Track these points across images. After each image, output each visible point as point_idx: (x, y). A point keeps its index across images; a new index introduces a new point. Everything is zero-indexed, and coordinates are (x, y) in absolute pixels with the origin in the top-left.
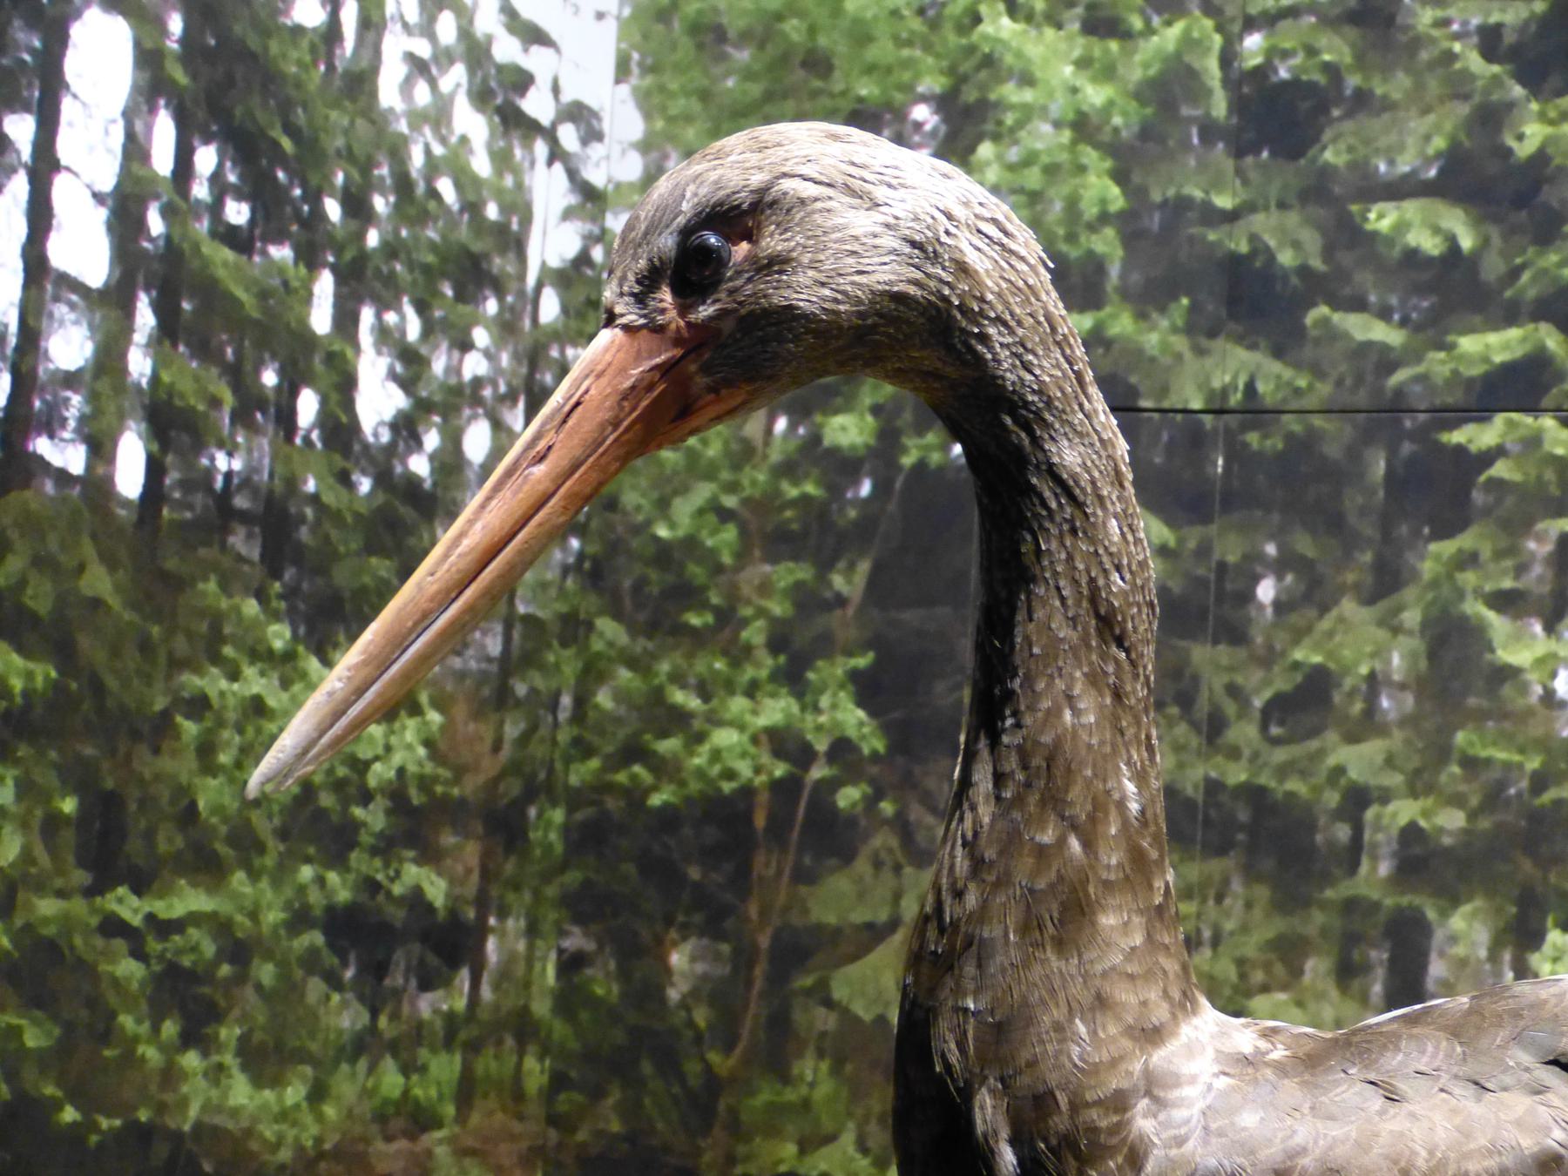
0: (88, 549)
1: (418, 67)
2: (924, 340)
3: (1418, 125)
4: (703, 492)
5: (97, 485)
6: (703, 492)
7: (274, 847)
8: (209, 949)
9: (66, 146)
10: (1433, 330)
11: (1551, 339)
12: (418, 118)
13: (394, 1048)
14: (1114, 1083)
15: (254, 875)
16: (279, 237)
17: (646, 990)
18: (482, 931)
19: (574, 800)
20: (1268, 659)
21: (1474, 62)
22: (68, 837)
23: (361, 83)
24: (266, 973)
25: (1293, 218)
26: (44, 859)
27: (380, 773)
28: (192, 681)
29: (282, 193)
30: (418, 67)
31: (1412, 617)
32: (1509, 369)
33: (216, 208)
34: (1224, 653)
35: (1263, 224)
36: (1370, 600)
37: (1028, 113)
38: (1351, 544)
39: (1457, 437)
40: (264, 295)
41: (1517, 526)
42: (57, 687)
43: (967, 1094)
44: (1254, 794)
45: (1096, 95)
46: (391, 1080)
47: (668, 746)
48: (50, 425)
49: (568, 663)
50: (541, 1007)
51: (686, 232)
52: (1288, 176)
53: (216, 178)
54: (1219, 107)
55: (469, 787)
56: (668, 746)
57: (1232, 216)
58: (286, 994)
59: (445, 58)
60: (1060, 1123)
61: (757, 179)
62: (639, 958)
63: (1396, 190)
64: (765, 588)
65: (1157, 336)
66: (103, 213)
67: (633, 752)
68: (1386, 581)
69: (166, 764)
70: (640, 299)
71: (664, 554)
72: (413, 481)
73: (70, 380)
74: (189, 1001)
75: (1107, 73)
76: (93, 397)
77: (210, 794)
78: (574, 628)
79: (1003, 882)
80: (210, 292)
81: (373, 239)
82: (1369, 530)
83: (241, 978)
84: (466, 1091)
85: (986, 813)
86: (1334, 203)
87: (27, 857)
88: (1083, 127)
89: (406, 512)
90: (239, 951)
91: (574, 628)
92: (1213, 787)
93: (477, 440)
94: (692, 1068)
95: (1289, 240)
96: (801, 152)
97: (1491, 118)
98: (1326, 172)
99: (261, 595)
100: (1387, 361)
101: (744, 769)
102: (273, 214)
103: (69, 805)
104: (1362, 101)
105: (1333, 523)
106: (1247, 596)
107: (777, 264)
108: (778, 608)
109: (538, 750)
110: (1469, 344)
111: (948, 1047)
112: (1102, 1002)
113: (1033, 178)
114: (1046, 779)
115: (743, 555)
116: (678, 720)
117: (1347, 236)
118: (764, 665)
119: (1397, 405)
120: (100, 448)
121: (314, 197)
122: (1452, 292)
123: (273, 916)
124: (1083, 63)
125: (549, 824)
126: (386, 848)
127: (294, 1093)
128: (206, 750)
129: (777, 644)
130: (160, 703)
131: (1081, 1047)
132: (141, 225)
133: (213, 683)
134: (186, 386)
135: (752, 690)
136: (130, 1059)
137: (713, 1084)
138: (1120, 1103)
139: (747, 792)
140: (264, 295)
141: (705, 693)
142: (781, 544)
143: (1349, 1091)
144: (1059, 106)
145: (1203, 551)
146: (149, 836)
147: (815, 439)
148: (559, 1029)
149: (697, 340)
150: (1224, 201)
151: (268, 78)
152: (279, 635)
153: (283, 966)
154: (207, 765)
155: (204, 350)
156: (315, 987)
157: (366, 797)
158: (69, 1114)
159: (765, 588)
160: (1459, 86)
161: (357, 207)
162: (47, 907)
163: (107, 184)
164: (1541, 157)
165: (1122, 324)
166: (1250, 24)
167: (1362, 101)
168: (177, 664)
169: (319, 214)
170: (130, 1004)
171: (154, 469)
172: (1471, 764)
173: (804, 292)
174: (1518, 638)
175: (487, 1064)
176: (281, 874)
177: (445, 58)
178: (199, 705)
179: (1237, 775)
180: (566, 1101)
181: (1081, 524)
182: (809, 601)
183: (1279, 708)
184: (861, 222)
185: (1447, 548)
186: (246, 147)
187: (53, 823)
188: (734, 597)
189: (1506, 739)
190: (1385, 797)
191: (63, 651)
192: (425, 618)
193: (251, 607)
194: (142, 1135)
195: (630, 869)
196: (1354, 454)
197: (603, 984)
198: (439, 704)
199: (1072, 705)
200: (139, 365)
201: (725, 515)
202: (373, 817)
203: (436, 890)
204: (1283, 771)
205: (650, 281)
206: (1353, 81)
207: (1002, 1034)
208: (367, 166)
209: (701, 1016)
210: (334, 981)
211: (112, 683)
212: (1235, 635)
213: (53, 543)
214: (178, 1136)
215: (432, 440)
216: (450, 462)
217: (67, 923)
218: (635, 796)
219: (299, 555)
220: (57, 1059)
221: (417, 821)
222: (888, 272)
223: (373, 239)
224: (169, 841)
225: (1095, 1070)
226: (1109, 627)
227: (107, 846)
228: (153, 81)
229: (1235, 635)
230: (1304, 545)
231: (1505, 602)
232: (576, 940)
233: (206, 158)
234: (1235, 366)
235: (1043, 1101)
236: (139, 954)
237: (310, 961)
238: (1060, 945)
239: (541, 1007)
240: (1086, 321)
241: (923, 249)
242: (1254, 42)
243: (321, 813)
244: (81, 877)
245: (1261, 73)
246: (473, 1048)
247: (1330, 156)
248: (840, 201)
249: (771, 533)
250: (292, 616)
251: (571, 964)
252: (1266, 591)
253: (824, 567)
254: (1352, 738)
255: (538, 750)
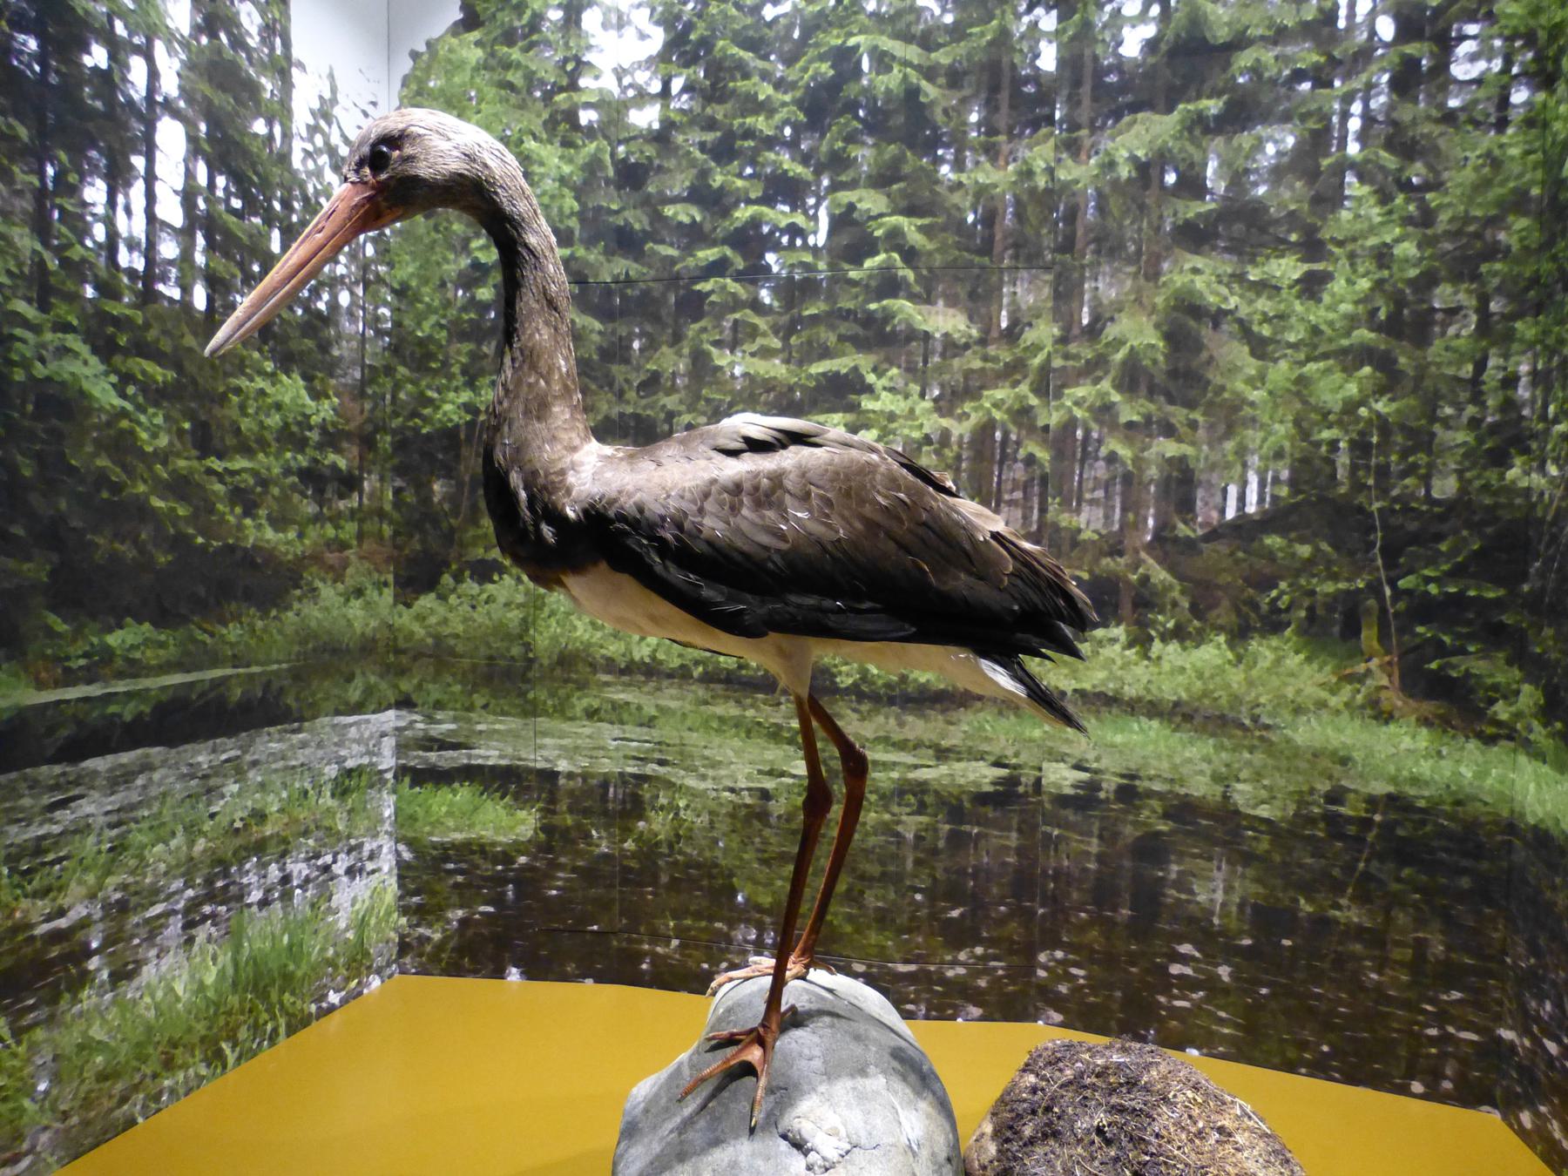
0: (185, 329)
1: (308, 154)
2: (471, 195)
3: (680, 177)
4: (433, 319)
5: (186, 304)
6: (433, 319)
7: (275, 445)
8: (251, 481)
9: (159, 170)
10: (688, 250)
11: (728, 252)
12: (309, 174)
13: (330, 519)
14: (560, 466)
15: (267, 455)
16: (256, 214)
17: (426, 500)
18: (361, 479)
19: (394, 432)
20: (638, 369)
21: (698, 154)
22: (188, 438)
23: (284, 158)
24: (276, 491)
25: (639, 212)
26: (178, 445)
27: (315, 420)
28: (234, 381)
29: (255, 198)
30: (308, 154)
31: (686, 351)
32: (714, 263)
33: (227, 201)
34: (623, 368)
35: (629, 215)
36: (671, 345)
37: (543, 176)
38: (664, 326)
39: (698, 287)
40: (251, 236)
41: (719, 317)
42: (177, 381)
43: (507, 473)
44: (636, 416)
45: (567, 169)
46: (330, 531)
47: (427, 411)
48: (164, 279)
49: (389, 385)
50: (388, 507)
51: (374, 146)
52: (637, 196)
53: (226, 189)
54: (611, 172)
55: (352, 426)
56: (427, 411)
57: (617, 212)
58: (284, 499)
59: (319, 152)
60: (541, 481)
61: (401, 126)
62: (423, 488)
63: (674, 200)
64: (459, 352)
65: (594, 256)
66: (178, 199)
67: (415, 414)
68: (677, 339)
69: (226, 412)
70: (357, 172)
71: (421, 342)
72: (319, 312)
73: (171, 262)
74: (246, 500)
75: (570, 161)
76: (181, 270)
77: (246, 424)
78: (389, 371)
79: (516, 397)
80: (228, 234)
81: (295, 218)
82: (670, 321)
83: (266, 492)
84: (360, 536)
85: (509, 373)
86: (652, 206)
87: (171, 443)
88: (563, 180)
89: (318, 323)
90: (264, 483)
91: (389, 371)
92: (622, 415)
93: (344, 299)
94: (444, 525)
95: (637, 220)
96: (422, 119)
97: (704, 174)
98: (649, 195)
99: (260, 350)
100: (672, 261)
101: (455, 418)
102: (251, 206)
103: (187, 426)
104: (660, 169)
105: (656, 319)
106: (630, 347)
107: (410, 159)
108: (464, 360)
109: (378, 414)
110: (700, 254)
111: (499, 456)
112: (554, 438)
113: (546, 200)
114: (531, 359)
115: (449, 341)
116: (430, 401)
117: (657, 217)
118: (460, 380)
119: (678, 277)
120: (186, 290)
121: (269, 200)
122: (694, 236)
123: (276, 471)
124: (561, 158)
125: (385, 441)
126: (320, 447)
127: (292, 535)
128: (243, 408)
129: (464, 372)
130: (221, 389)
131: (547, 454)
132: (195, 206)
133: (243, 382)
134: (221, 268)
135: (456, 390)
136: (222, 521)
137: (452, 530)
138: (562, 472)
139: (457, 426)
140: (251, 236)
141: (439, 391)
142: (463, 336)
143: (646, 465)
144: (554, 173)
145: (613, 332)
146: (222, 439)
147: (473, 298)
148: (396, 515)
149: (380, 188)
150: (614, 207)
151: (245, 153)
152: (269, 366)
153: (282, 490)
154: (244, 414)
155: (227, 255)
156: (296, 497)
157: (310, 428)
158: (200, 540)
159: (459, 352)
160: (693, 163)
161: (287, 205)
162: (182, 463)
163: (180, 187)
164: (722, 188)
165: (581, 252)
166: (620, 142)
167: (660, 169)
168: (227, 375)
169: (271, 206)
170: (221, 500)
171: (210, 300)
172: (708, 401)
173: (423, 170)
174: (722, 356)
175: (368, 526)
176: (278, 455)
177: (319, 152)
178: (238, 391)
179: (629, 410)
180: (399, 540)
181: (538, 266)
182: (475, 356)
183: (643, 386)
184: (444, 145)
185: (696, 326)
186: (236, 177)
187: (181, 433)
188: (447, 357)
189: (719, 391)
190: (680, 414)
191: (179, 367)
192: (275, 290)
193: (256, 355)
194: (231, 549)
195: (416, 456)
196: (664, 295)
197: (410, 497)
198: (337, 395)
199: (539, 332)
200: (200, 259)
201: (442, 327)
202: (314, 436)
203: (342, 463)
204: (645, 408)
205: (360, 164)
206: (657, 162)
207: (519, 449)
208: (290, 190)
209: (446, 507)
210: (304, 495)
211: (201, 381)
212: (626, 361)
213: (169, 325)
214: (245, 550)
215: (326, 297)
216: (334, 305)
217: (191, 471)
218: (416, 430)
219: (275, 336)
220: (193, 519)
221: (332, 438)
222: (456, 165)
223: (295, 218)
224: (230, 441)
225: (553, 461)
226: (551, 304)
227: (204, 441)
228: (195, 148)
229: (626, 361)
230: (649, 328)
231: (717, 344)
232: (399, 483)
233: (221, 181)
234: (622, 266)
235: (535, 473)
236: (222, 481)
237: (293, 487)
238: (539, 419)
239: (388, 507)
240: (567, 252)
241: (470, 157)
242: (621, 149)
243: (292, 434)
244: (194, 453)
245: (624, 161)
246: (361, 521)
247: (651, 189)
248: (435, 137)
249: (460, 332)
250: (273, 359)
251: (398, 492)
252: (636, 345)
253: (479, 344)
254: (668, 394)
255: (378, 414)
